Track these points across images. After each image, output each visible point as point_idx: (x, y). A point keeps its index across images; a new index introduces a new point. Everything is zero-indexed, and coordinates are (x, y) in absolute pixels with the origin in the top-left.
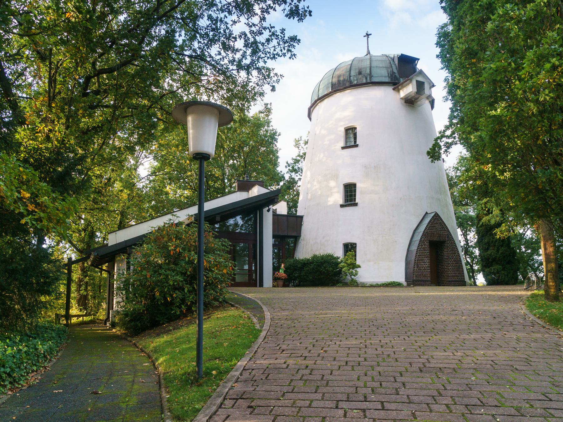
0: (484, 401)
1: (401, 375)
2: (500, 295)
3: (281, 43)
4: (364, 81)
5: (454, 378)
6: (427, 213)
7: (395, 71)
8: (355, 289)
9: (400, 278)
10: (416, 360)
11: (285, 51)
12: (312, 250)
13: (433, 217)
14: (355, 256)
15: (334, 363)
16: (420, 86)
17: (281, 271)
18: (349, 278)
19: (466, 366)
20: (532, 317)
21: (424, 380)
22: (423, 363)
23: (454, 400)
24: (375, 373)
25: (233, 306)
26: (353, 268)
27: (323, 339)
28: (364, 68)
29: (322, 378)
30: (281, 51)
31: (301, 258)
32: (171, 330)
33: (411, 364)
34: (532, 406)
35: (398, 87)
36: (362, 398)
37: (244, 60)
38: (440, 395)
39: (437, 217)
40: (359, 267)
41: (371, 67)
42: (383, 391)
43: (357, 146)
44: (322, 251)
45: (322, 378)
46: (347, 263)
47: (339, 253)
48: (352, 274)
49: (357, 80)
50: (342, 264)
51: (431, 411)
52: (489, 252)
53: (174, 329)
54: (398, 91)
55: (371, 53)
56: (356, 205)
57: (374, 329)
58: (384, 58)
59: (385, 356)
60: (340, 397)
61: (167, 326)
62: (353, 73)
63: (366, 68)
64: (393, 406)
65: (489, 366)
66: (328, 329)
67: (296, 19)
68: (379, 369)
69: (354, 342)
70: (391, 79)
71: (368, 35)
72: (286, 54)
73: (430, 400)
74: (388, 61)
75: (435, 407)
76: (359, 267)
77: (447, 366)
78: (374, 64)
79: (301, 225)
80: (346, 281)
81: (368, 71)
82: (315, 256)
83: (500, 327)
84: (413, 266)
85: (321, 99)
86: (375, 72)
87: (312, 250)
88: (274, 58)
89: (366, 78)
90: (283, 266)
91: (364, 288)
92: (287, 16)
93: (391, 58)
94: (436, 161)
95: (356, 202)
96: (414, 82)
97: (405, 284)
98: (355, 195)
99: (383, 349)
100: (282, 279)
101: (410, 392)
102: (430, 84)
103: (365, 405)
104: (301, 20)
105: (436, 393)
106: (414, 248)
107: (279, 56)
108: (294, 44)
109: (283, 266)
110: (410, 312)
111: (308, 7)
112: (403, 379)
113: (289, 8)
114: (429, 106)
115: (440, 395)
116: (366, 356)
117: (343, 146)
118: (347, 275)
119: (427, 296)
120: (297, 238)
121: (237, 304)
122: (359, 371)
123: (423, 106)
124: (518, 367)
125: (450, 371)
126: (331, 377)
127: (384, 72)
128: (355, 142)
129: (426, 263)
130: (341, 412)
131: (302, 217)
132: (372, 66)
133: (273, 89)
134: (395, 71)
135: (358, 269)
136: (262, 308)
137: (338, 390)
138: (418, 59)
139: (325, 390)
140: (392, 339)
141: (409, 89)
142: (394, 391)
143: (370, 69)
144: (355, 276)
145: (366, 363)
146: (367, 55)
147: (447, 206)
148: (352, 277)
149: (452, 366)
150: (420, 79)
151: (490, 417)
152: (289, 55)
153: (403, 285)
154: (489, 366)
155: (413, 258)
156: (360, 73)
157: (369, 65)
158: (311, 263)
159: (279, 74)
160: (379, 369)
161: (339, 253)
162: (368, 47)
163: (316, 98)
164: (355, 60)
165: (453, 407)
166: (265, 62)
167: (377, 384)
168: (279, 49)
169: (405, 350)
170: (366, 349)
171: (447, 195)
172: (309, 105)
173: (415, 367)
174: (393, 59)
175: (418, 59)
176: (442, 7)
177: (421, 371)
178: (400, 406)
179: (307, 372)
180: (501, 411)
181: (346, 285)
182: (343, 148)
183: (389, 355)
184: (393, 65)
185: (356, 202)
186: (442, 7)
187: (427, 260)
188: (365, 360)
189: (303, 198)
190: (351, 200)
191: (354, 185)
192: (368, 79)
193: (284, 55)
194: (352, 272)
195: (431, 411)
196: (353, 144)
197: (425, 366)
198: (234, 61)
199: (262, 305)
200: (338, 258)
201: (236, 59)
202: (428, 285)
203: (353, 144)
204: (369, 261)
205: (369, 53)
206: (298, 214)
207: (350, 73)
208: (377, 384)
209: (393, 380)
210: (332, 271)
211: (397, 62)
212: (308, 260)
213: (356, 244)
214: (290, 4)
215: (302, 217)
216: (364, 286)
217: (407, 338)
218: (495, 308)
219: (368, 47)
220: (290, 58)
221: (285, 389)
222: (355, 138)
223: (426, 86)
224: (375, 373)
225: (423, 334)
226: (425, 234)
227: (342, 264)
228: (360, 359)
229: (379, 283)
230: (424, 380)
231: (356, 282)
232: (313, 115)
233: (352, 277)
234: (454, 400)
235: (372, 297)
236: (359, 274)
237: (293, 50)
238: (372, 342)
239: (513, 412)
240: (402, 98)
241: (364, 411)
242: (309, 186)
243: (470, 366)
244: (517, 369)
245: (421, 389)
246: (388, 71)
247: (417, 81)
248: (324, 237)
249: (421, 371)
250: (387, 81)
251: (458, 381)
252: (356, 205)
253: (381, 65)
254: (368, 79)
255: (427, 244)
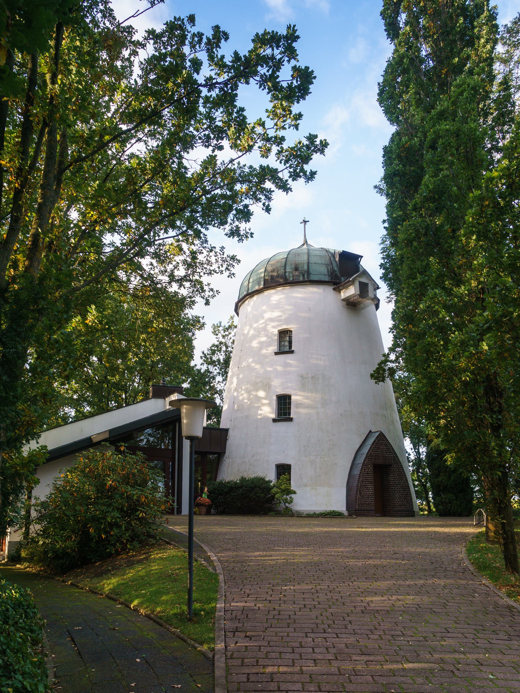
0: (404, 632)
1: (348, 616)
2: (446, 533)
3: (219, 261)
4: (301, 279)
5: (387, 618)
6: (370, 431)
7: (336, 269)
8: (292, 521)
9: (340, 506)
10: (359, 604)
11: (223, 269)
12: (238, 470)
13: (378, 437)
14: (290, 480)
15: (295, 606)
16: (364, 288)
17: (204, 495)
18: (283, 505)
19: (397, 609)
20: (467, 563)
21: (365, 619)
22: (365, 607)
23: (384, 632)
24: (328, 614)
25: (168, 543)
26: (288, 494)
27: (278, 584)
28: (301, 264)
29: (290, 618)
30: (219, 268)
31: (227, 480)
32: (109, 571)
33: (355, 607)
34: (435, 636)
35: (339, 287)
36: (322, 631)
37: (175, 271)
38: (376, 629)
39: (381, 437)
40: (295, 493)
41: (308, 263)
42: (336, 626)
43: (292, 352)
44: (251, 474)
45: (290, 618)
46: (280, 489)
47: (271, 476)
48: (286, 501)
49: (293, 276)
50: (275, 489)
51: (369, 639)
52: (440, 479)
53: (113, 569)
54: (339, 292)
55: (309, 242)
56: (291, 420)
57: (321, 574)
58: (324, 253)
59: (335, 601)
60: (306, 630)
61: (101, 566)
62: (288, 270)
63: (304, 264)
64: (344, 636)
65: (414, 609)
66: (279, 573)
67: (236, 239)
68: (331, 610)
69: (306, 587)
70: (332, 278)
71: (305, 222)
72: (224, 272)
73: (368, 632)
74: (328, 258)
75: (372, 636)
76: (295, 493)
77: (382, 608)
78: (313, 260)
79: (226, 440)
80: (279, 509)
81: (306, 267)
82: (243, 479)
83: (433, 573)
84: (355, 492)
85: (250, 295)
86: (313, 268)
87: (238, 470)
88: (210, 273)
89: (303, 276)
90: (206, 489)
91: (300, 519)
92: (226, 235)
93: (332, 254)
94: (381, 383)
95: (291, 416)
96: (357, 284)
97: (346, 513)
98: (290, 408)
99: (331, 594)
100: (205, 506)
101: (355, 627)
102: (374, 286)
103: (326, 635)
104: (241, 240)
105: (373, 628)
106: (357, 472)
107: (216, 272)
108: (234, 264)
109: (206, 489)
110: (353, 554)
111: (250, 230)
112: (349, 618)
113: (230, 228)
114: (374, 307)
115: (376, 629)
116: (318, 600)
117: (276, 351)
118: (280, 502)
119: (372, 533)
120: (221, 454)
121: (173, 541)
122: (315, 613)
123: (368, 309)
124: (435, 610)
125: (384, 612)
126: (296, 617)
127: (323, 270)
128: (290, 347)
129: (370, 490)
130: (310, 639)
131: (226, 431)
132: (310, 262)
133: (207, 303)
134: (336, 269)
135: (293, 496)
136: (202, 548)
137: (304, 625)
138: (362, 257)
139: (295, 626)
140: (338, 585)
141: (351, 291)
142: (344, 627)
143: (308, 266)
144: (289, 503)
145: (320, 606)
146: (304, 244)
147: (393, 422)
148: (287, 504)
149: (386, 609)
150: (364, 280)
151: (406, 642)
152: (228, 273)
153: (344, 515)
154: (414, 609)
155: (355, 484)
156: (296, 269)
157: (306, 261)
158: (241, 487)
159: (215, 290)
160: (331, 610)
161: (271, 476)
162: (305, 235)
163: (245, 293)
164: (291, 253)
165: (383, 637)
166: (200, 276)
167: (331, 622)
168: (217, 265)
169: (350, 595)
170: (318, 594)
171: (393, 410)
172: (236, 300)
173: (359, 609)
174: (333, 255)
175: (362, 257)
176: (385, 228)
177: (363, 612)
178: (349, 636)
179: (276, 613)
180: (414, 639)
181: (279, 514)
182: (276, 354)
183: (337, 600)
184: (333, 262)
185: (291, 416)
186: (385, 228)
187: (371, 487)
188: (319, 604)
189: (229, 407)
190: (285, 414)
191: (289, 397)
192: (306, 276)
193: (222, 272)
194: (287, 499)
195: (369, 639)
196: (287, 349)
197: (366, 609)
198: (166, 271)
199: (200, 543)
200: (271, 482)
201: (169, 270)
202: (372, 516)
203: (287, 349)
204: (306, 486)
205: (306, 242)
206: (222, 426)
207: (285, 269)
208: (331, 622)
209: (342, 619)
210: (264, 497)
211: (337, 259)
212: (236, 483)
213: (290, 465)
214: (231, 224)
215: (226, 431)
216: (299, 515)
217: (351, 584)
218: (437, 550)
219: (305, 235)
220: (228, 277)
221: (266, 625)
222: (290, 342)
223: (371, 288)
224: (328, 614)
225: (365, 580)
226: (369, 456)
227: (275, 489)
228: (315, 603)
229: (317, 513)
230: (365, 619)
231: (291, 510)
232: (241, 310)
233: (287, 504)
234: (384, 632)
235: (311, 533)
236: (294, 502)
237: (232, 269)
238: (322, 587)
239: (421, 639)
240: (343, 300)
241: (325, 638)
242: (235, 394)
243: (400, 609)
244: (434, 611)
245: (363, 625)
246: (328, 269)
247: (361, 283)
248: (253, 456)
249: (363, 612)
250: (327, 280)
251: (389, 620)
252: (291, 420)
253: (320, 262)
254: (306, 276)
255: (371, 467)
